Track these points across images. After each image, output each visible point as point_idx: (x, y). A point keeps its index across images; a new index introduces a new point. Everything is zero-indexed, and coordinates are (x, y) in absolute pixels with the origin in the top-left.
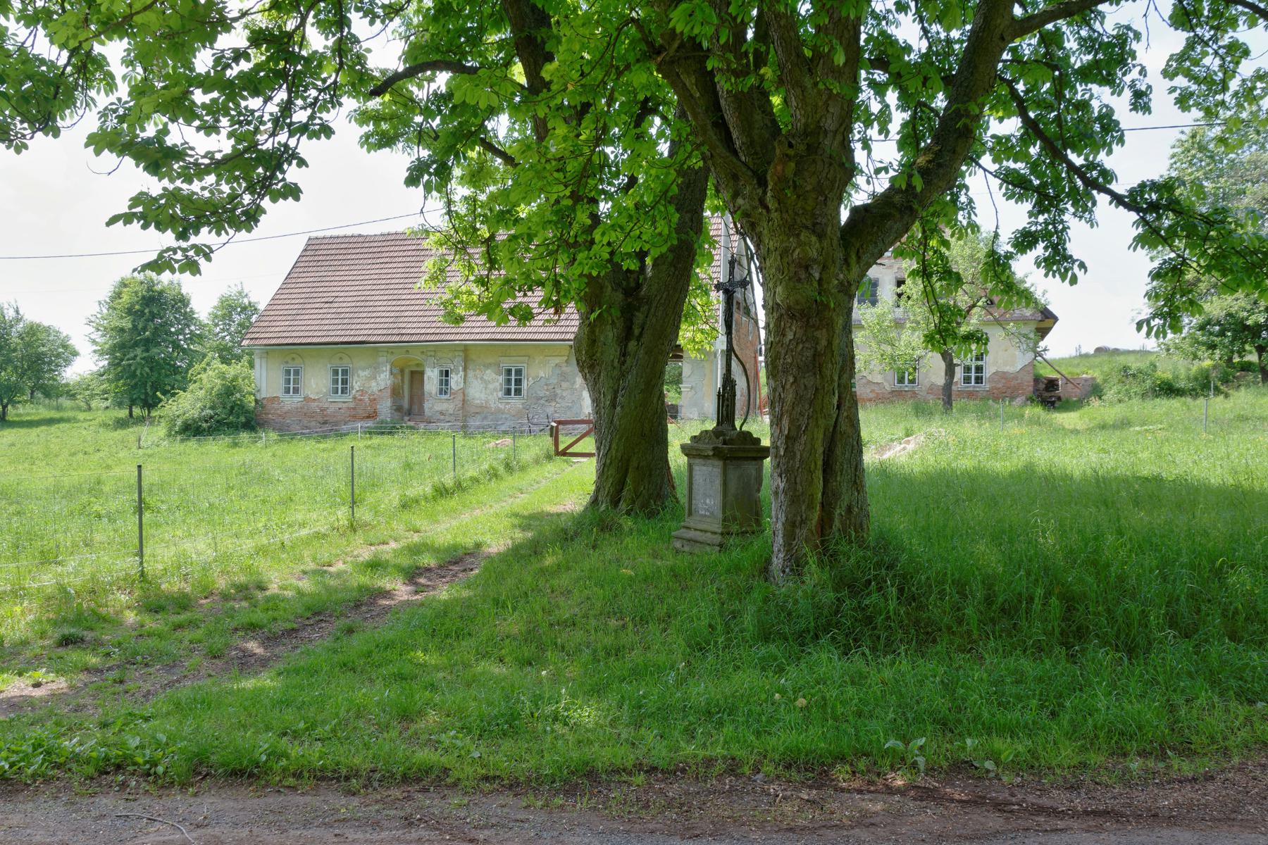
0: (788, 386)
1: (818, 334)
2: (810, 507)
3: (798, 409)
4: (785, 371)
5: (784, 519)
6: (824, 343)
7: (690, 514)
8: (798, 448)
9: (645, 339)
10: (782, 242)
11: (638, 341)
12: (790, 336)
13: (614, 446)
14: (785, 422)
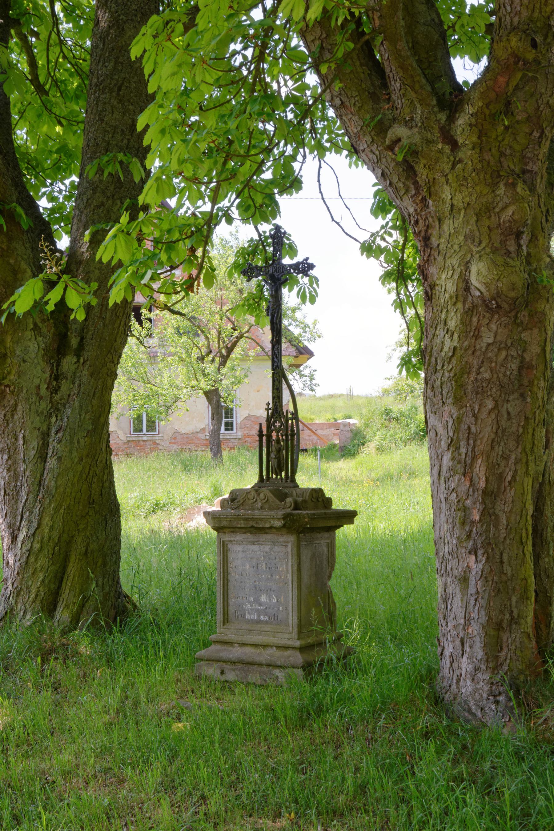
0: (484, 415)
1: (525, 336)
2: (524, 597)
3: (499, 450)
4: (480, 392)
5: (484, 619)
6: (535, 349)
7: (226, 620)
8: (502, 508)
9: (89, 353)
10: (480, 195)
11: (78, 356)
12: (487, 338)
13: (47, 520)
14: (480, 470)
